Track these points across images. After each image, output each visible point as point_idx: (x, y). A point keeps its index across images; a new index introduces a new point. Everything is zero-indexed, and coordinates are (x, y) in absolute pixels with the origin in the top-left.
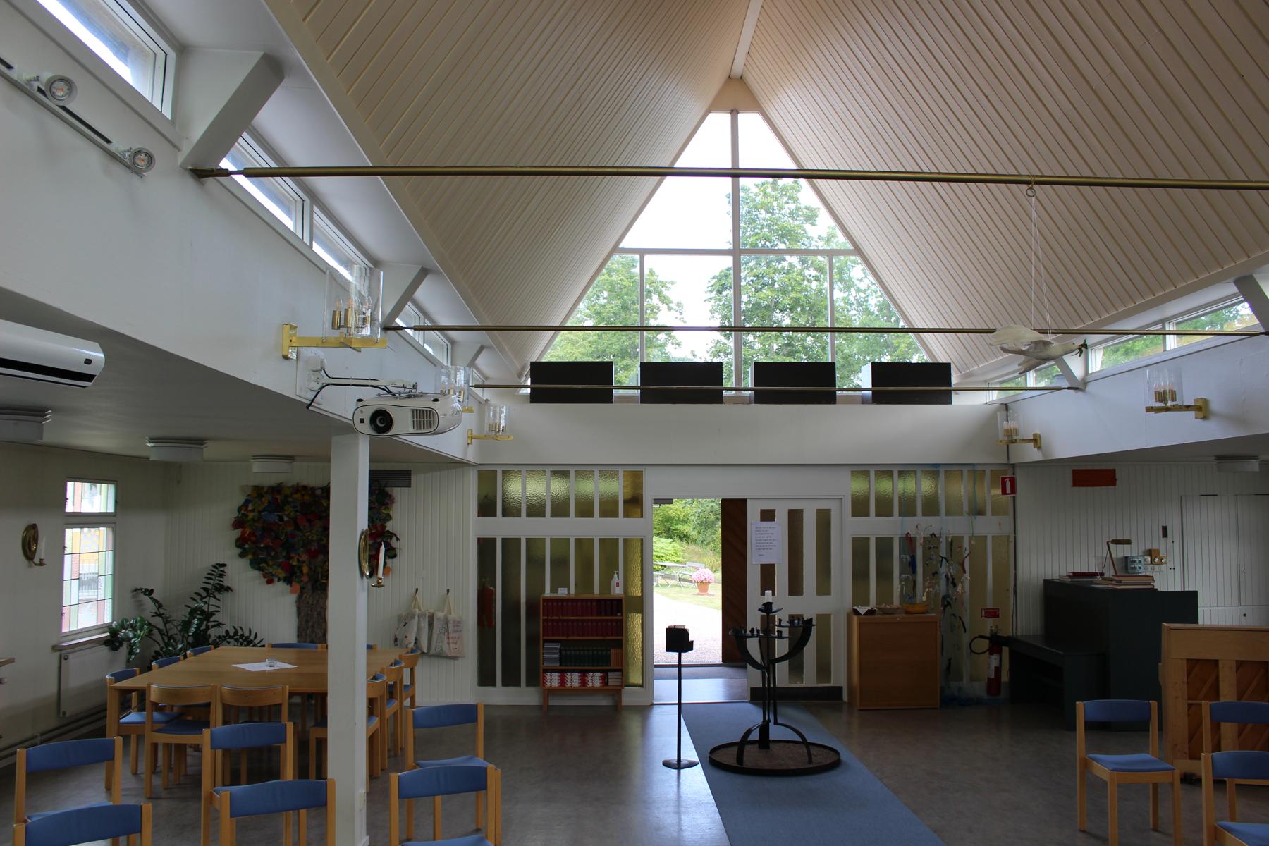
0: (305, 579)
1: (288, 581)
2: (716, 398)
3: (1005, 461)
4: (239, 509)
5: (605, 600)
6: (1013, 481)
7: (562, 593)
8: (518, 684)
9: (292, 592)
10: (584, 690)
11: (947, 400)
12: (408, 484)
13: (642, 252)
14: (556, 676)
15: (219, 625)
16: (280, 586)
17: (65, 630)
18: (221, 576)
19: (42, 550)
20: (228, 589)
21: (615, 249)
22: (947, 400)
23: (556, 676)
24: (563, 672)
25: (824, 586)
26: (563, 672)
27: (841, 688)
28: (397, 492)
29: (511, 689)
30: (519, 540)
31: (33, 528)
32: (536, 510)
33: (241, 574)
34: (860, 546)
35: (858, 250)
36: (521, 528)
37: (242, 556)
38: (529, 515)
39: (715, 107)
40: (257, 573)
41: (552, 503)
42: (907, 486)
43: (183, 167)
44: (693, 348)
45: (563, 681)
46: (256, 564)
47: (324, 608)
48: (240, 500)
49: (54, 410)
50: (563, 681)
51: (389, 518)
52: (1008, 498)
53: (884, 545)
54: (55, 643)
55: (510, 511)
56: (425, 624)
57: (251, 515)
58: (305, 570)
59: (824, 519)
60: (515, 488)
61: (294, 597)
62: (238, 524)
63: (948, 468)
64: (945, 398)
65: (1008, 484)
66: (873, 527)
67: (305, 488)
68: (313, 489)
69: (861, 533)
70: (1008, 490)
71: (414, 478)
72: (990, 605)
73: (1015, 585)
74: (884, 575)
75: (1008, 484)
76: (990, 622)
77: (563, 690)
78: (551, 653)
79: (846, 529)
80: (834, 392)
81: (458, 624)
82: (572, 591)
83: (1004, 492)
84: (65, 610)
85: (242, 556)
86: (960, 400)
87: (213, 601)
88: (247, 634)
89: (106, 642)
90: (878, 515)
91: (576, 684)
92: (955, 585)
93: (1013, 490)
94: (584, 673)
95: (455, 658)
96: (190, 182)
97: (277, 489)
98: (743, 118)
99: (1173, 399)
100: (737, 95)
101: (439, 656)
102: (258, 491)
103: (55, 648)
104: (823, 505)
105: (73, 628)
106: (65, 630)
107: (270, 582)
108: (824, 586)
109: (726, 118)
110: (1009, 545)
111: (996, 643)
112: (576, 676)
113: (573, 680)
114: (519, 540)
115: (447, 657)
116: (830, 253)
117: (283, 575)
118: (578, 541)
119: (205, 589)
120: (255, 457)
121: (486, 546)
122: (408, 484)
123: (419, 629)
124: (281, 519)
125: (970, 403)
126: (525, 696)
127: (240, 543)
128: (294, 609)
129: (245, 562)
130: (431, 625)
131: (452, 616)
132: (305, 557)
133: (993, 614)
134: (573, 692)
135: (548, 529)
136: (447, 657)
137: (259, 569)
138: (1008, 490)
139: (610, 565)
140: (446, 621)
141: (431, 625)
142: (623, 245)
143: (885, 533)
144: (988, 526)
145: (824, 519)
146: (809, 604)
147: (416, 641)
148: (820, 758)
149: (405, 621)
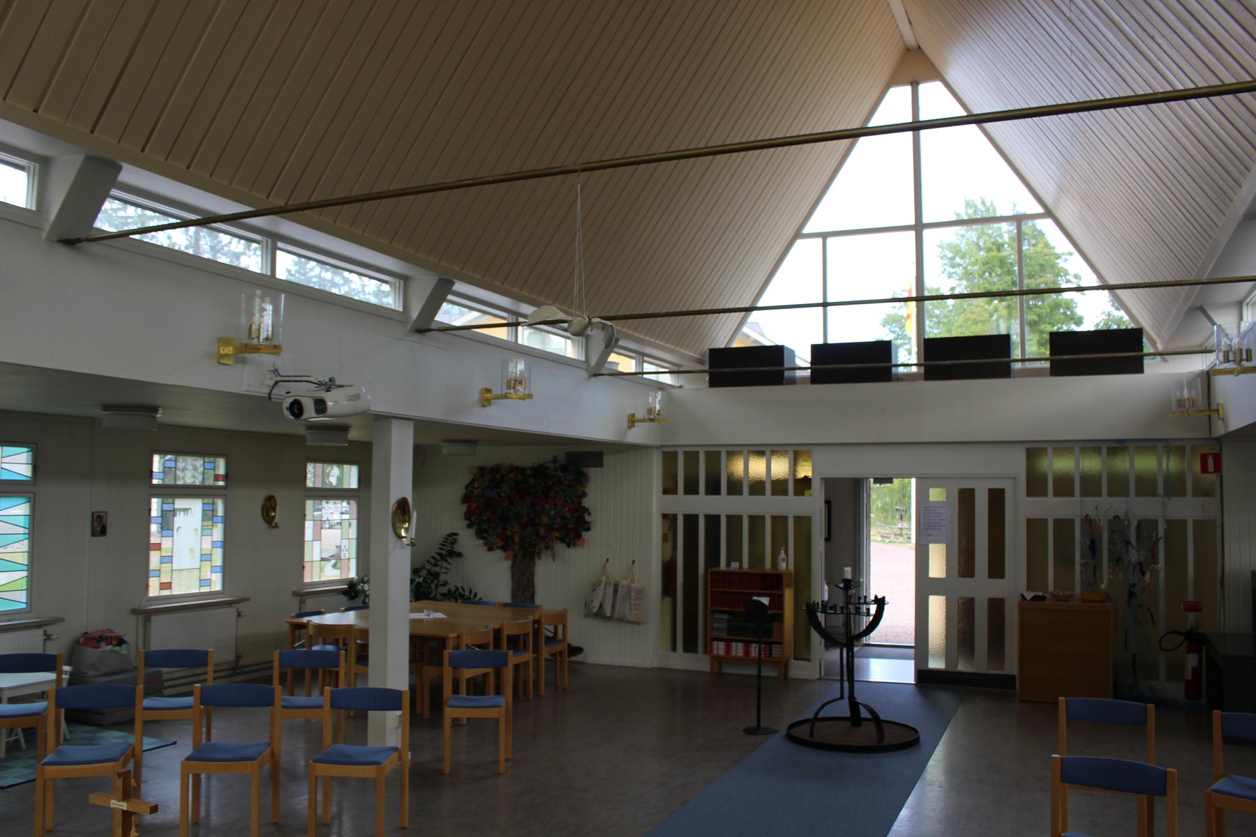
0: (517, 547)
1: (504, 548)
2: (1004, 371)
3: (1204, 434)
4: (467, 487)
5: (756, 575)
6: (1217, 458)
7: (735, 565)
8: (695, 651)
9: (506, 558)
10: (745, 660)
11: (1140, 370)
12: (601, 465)
13: (825, 236)
14: (722, 645)
15: (446, 583)
16: (499, 553)
17: (307, 580)
18: (453, 543)
19: (278, 515)
20: (460, 555)
21: (798, 235)
22: (1140, 370)
23: (722, 645)
24: (728, 642)
25: (997, 569)
26: (728, 642)
27: (1013, 677)
28: (593, 472)
29: (690, 655)
30: (1046, 521)
31: (270, 499)
32: (757, 487)
33: (469, 542)
34: (1035, 527)
35: (1049, 213)
36: (744, 505)
37: (469, 526)
38: (774, 493)
39: (894, 81)
40: (481, 542)
41: (1055, 481)
42: (1146, 463)
43: (48, 239)
44: (1094, 312)
45: (728, 650)
46: (480, 534)
47: (533, 574)
48: (467, 479)
49: (164, 408)
50: (728, 650)
51: (584, 495)
52: (1211, 477)
53: (1063, 526)
54: (296, 589)
55: (735, 487)
56: (610, 590)
57: (476, 492)
58: (517, 539)
59: (997, 497)
60: (738, 467)
61: (509, 563)
62: (466, 499)
63: (730, 449)
64: (1136, 366)
65: (1210, 461)
66: (1050, 507)
67: (517, 468)
68: (524, 470)
69: (1036, 514)
70: (1211, 467)
71: (605, 459)
72: (1191, 597)
73: (1223, 577)
74: (1064, 558)
75: (1210, 461)
76: (1191, 617)
77: (728, 659)
78: (721, 622)
79: (1020, 509)
80: (782, 372)
81: (640, 592)
82: (746, 565)
83: (1204, 469)
84: (306, 565)
85: (469, 526)
86: (1154, 369)
87: (445, 564)
88: (467, 593)
89: (344, 592)
90: (1109, 495)
91: (740, 653)
92: (1143, 573)
93: (1218, 468)
94: (747, 644)
95: (638, 623)
96: (64, 251)
97: (496, 469)
98: (923, 88)
99: (1249, 359)
100: (915, 66)
101: (622, 620)
102: (482, 471)
103: (296, 594)
104: (967, 485)
105: (316, 579)
106: (307, 580)
107: (490, 549)
108: (997, 569)
109: (907, 90)
110: (1210, 533)
111: (1195, 640)
112: (740, 645)
113: (738, 649)
114: (1046, 521)
115: (629, 622)
116: (1019, 219)
117: (500, 543)
118: (797, 519)
119: (440, 554)
120: (445, 441)
121: (669, 519)
122: (601, 465)
123: (604, 594)
124: (499, 495)
125: (1166, 372)
126: (698, 663)
127: (468, 516)
128: (509, 574)
129: (471, 532)
130: (615, 591)
131: (636, 585)
132: (516, 529)
133: (1195, 608)
134: (737, 661)
135: (768, 506)
136: (629, 622)
137: (482, 538)
138: (1211, 467)
139: (779, 541)
140: (629, 589)
141: (615, 591)
142: (805, 231)
143: (1063, 515)
144: (1187, 509)
145: (997, 497)
146: (997, 588)
147: (601, 606)
148: (891, 737)
149: (595, 587)
